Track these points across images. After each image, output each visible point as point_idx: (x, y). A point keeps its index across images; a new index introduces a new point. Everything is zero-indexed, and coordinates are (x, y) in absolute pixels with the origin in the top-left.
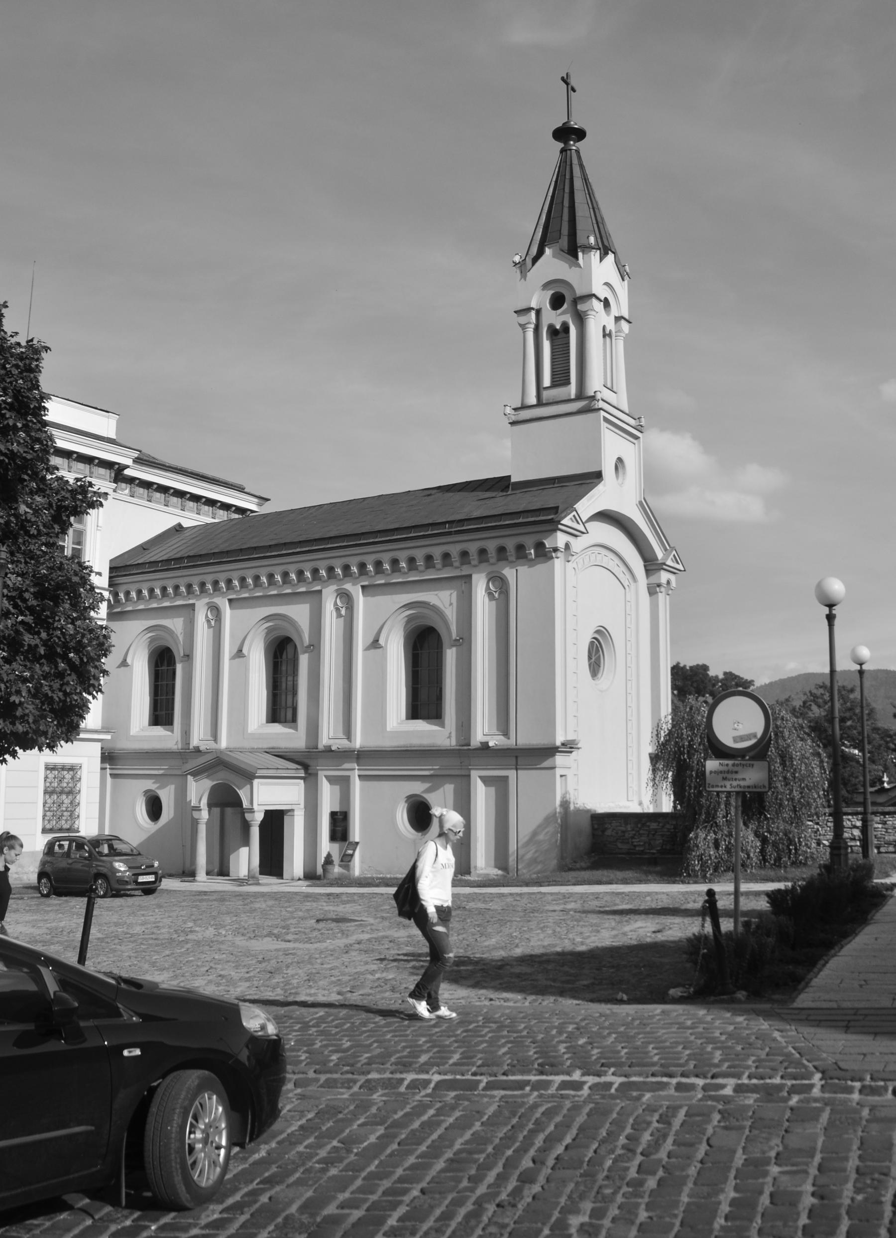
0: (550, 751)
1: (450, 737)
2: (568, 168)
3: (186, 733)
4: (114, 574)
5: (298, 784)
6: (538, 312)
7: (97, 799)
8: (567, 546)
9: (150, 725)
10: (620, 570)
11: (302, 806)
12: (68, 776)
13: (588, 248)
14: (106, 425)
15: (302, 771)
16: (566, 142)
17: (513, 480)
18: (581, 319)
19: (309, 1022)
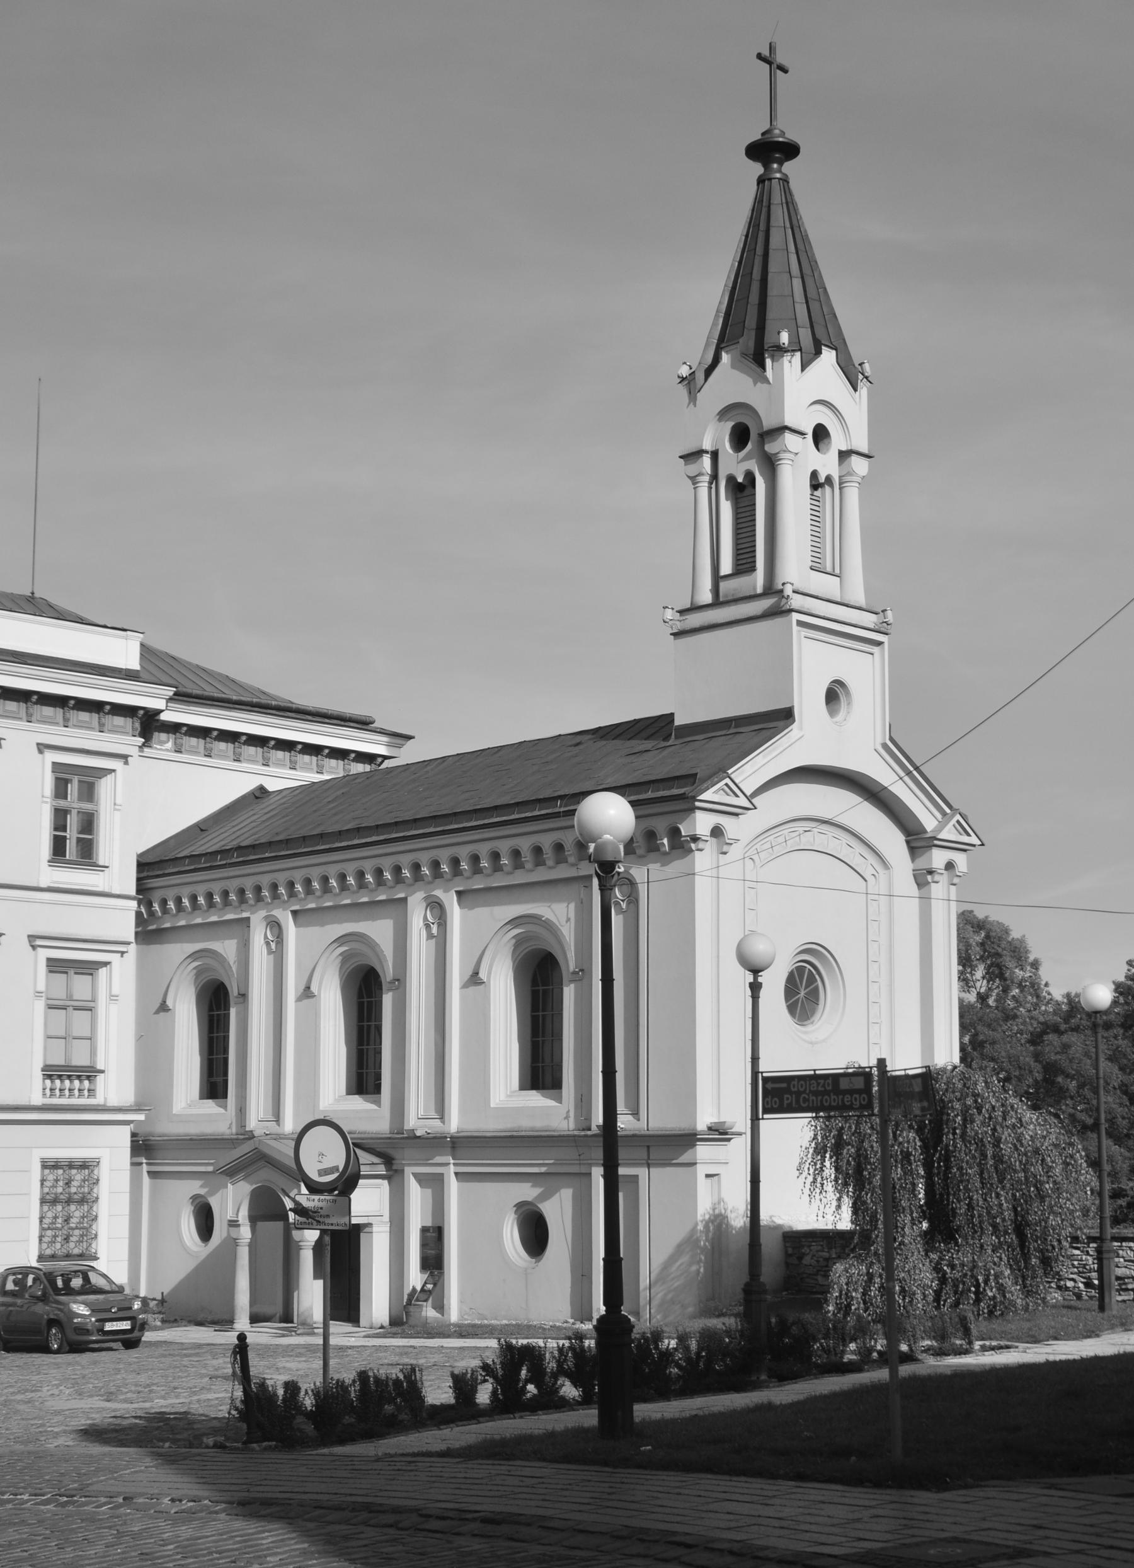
0: (688, 1139)
1: (567, 1118)
2: (764, 210)
3: (242, 1111)
4: (145, 874)
5: (378, 1187)
6: (715, 455)
7: (126, 1210)
8: (717, 832)
9: (201, 1098)
10: (854, 853)
11: (386, 1218)
12: (78, 1176)
13: (779, 350)
14: (124, 652)
15: (382, 1167)
16: (766, 165)
17: (678, 721)
18: (770, 464)
19: (224, 1510)
